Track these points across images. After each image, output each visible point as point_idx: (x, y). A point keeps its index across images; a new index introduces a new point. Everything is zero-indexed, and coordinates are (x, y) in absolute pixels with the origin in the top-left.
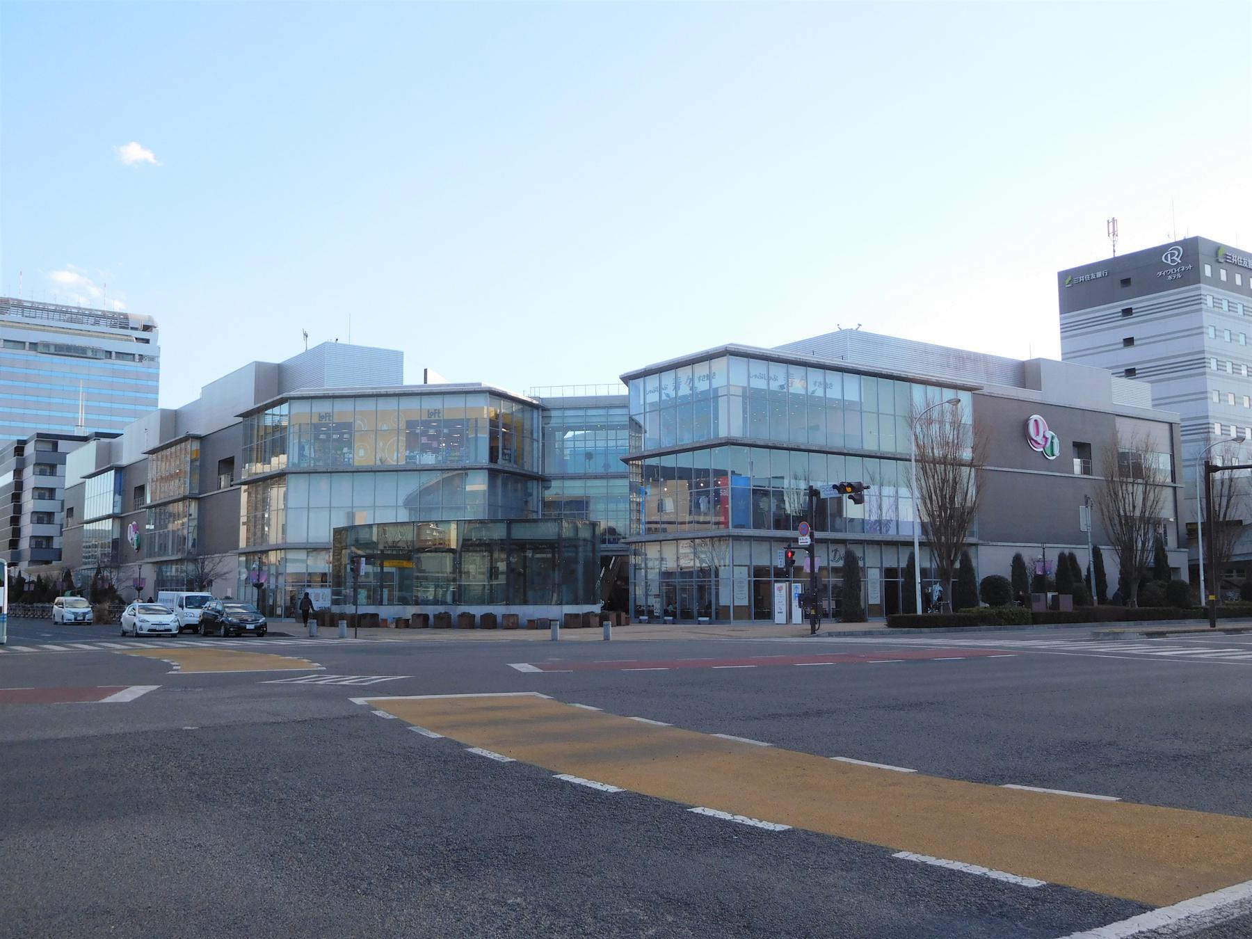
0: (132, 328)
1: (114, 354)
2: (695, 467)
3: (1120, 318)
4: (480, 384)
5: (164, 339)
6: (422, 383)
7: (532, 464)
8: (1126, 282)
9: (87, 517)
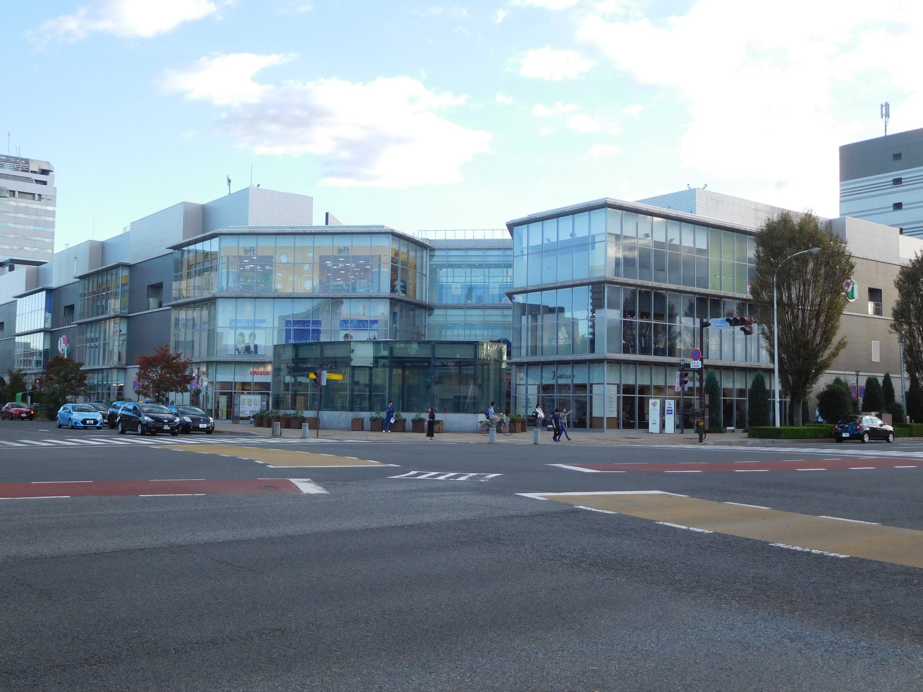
0: (32, 171)
1: (17, 194)
2: (528, 303)
3: (891, 186)
4: (383, 227)
5: (58, 180)
6: (324, 223)
7: (423, 295)
8: (897, 156)
9: (18, 331)
